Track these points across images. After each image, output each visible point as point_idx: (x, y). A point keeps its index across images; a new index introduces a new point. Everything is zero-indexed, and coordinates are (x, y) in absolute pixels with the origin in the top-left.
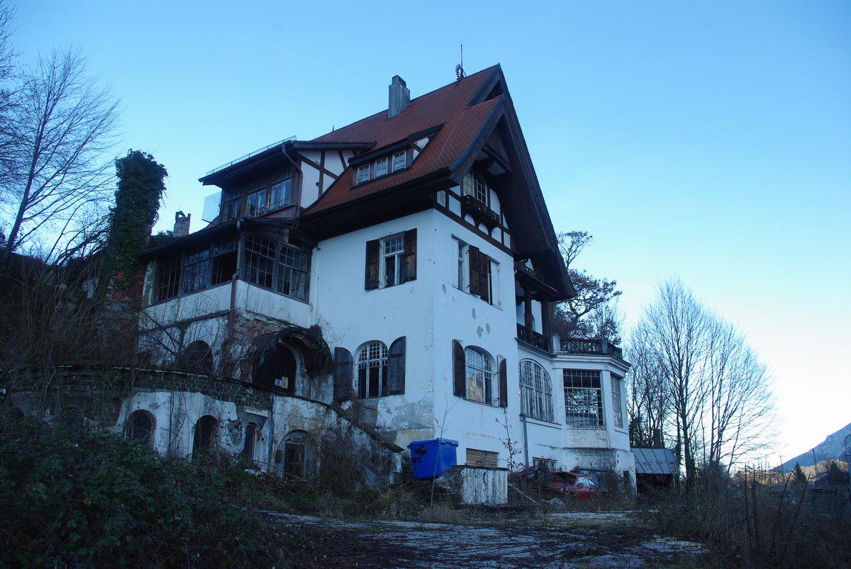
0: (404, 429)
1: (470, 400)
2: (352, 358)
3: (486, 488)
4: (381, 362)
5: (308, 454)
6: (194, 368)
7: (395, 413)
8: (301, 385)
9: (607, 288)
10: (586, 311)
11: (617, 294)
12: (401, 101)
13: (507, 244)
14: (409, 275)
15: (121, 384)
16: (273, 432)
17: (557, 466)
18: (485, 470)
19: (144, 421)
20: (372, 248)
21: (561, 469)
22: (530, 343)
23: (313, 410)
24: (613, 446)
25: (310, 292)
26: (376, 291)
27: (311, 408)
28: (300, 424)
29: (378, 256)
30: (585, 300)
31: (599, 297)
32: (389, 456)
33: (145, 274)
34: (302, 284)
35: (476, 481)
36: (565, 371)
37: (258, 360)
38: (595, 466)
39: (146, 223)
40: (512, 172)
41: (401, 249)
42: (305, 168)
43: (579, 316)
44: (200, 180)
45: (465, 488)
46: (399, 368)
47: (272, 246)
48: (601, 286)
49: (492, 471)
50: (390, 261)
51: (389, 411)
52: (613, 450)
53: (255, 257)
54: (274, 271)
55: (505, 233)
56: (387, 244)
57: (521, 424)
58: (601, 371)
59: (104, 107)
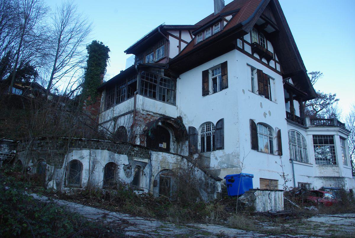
0: (225, 168)
1: (261, 152)
2: (197, 132)
3: (271, 202)
4: (212, 133)
5: (172, 182)
6: (119, 141)
7: (219, 160)
8: (173, 147)
9: (331, 98)
10: (321, 110)
11: (337, 100)
12: (220, 6)
13: (278, 69)
14: (224, 86)
15: (61, 146)
16: (151, 171)
17: (311, 187)
18: (270, 192)
19: (76, 166)
20: (205, 74)
21: (313, 188)
22: (294, 121)
23: (174, 159)
24: (343, 176)
25: (176, 99)
26: (208, 96)
27: (173, 157)
28: (167, 166)
29: (208, 78)
30: (320, 104)
31: (327, 102)
32: (214, 183)
33: (101, 97)
34: (173, 96)
35: (264, 198)
36: (314, 136)
37: (148, 133)
38: (333, 186)
39: (100, 73)
40: (279, 30)
41: (220, 73)
42: (171, 39)
43: (317, 112)
45: (257, 203)
46: (221, 135)
47: (155, 77)
48: (328, 97)
49: (274, 192)
50: (215, 80)
51: (216, 159)
52: (343, 178)
53: (146, 83)
54: (157, 90)
55: (275, 68)
56: (213, 72)
57: (290, 164)
58: (334, 135)
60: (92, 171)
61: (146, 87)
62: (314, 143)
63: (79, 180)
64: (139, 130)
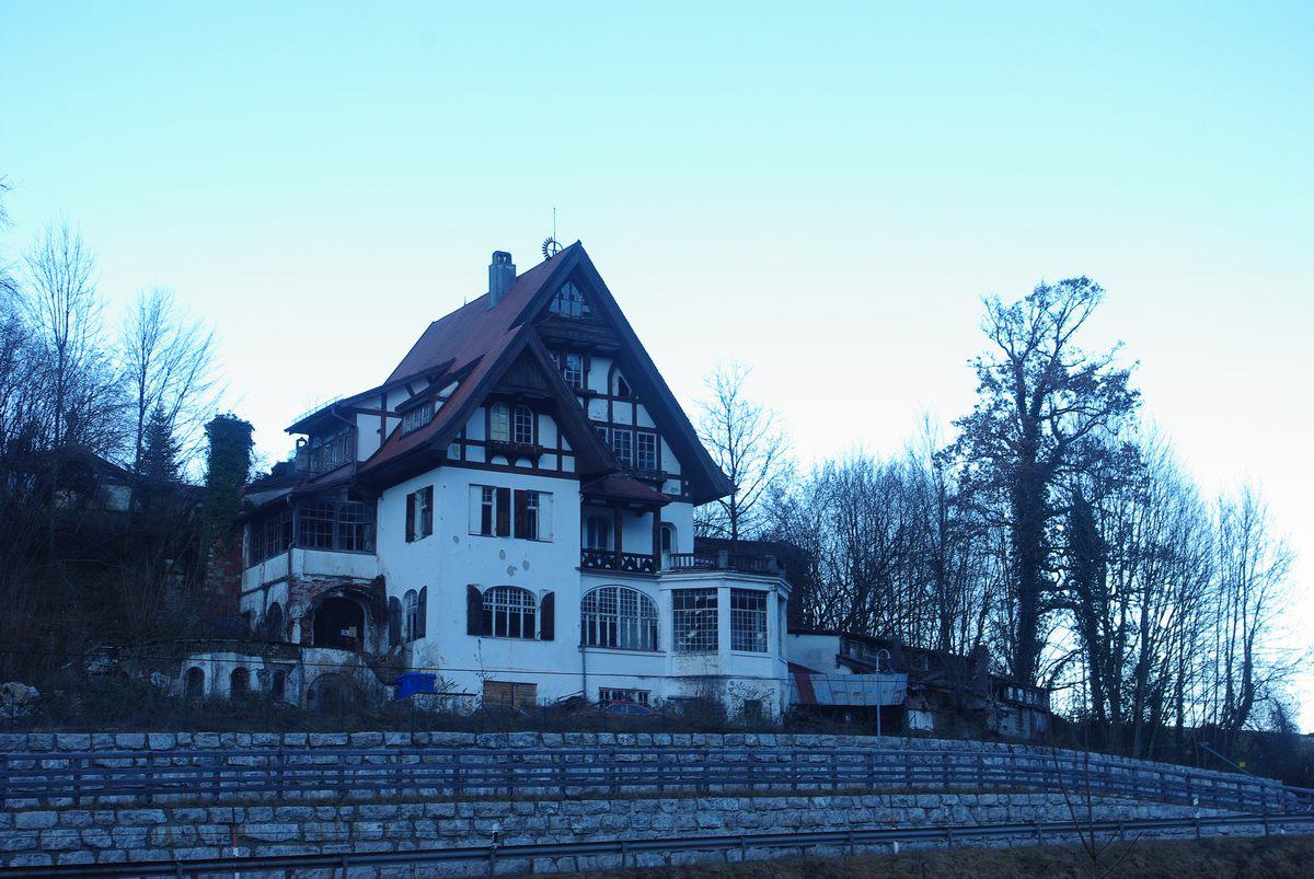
16: (303, 676)
19: (196, 674)
20: (411, 499)
36: (674, 592)
44: (286, 431)
59: (196, 346)
60: (215, 679)
61: (313, 530)
62: (732, 607)
63: (201, 690)
64: (297, 611)
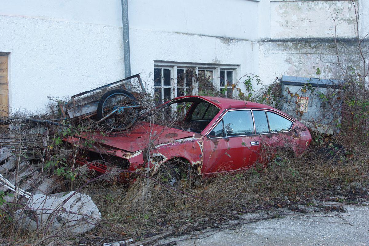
38: (325, 76)
